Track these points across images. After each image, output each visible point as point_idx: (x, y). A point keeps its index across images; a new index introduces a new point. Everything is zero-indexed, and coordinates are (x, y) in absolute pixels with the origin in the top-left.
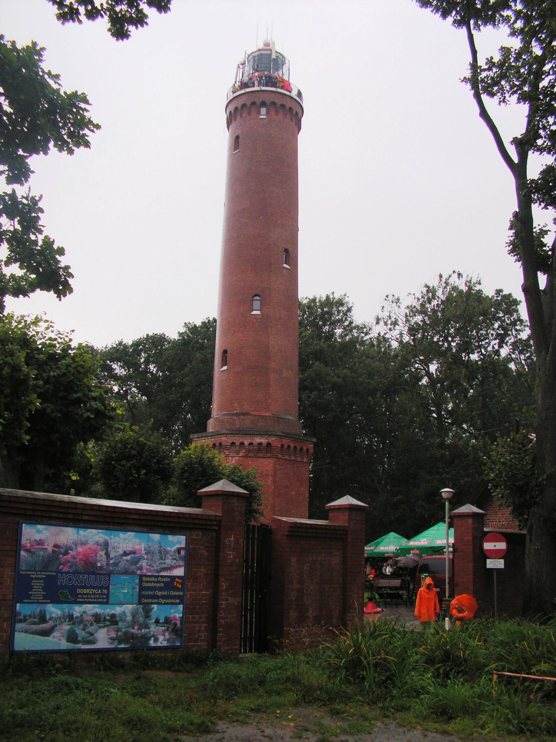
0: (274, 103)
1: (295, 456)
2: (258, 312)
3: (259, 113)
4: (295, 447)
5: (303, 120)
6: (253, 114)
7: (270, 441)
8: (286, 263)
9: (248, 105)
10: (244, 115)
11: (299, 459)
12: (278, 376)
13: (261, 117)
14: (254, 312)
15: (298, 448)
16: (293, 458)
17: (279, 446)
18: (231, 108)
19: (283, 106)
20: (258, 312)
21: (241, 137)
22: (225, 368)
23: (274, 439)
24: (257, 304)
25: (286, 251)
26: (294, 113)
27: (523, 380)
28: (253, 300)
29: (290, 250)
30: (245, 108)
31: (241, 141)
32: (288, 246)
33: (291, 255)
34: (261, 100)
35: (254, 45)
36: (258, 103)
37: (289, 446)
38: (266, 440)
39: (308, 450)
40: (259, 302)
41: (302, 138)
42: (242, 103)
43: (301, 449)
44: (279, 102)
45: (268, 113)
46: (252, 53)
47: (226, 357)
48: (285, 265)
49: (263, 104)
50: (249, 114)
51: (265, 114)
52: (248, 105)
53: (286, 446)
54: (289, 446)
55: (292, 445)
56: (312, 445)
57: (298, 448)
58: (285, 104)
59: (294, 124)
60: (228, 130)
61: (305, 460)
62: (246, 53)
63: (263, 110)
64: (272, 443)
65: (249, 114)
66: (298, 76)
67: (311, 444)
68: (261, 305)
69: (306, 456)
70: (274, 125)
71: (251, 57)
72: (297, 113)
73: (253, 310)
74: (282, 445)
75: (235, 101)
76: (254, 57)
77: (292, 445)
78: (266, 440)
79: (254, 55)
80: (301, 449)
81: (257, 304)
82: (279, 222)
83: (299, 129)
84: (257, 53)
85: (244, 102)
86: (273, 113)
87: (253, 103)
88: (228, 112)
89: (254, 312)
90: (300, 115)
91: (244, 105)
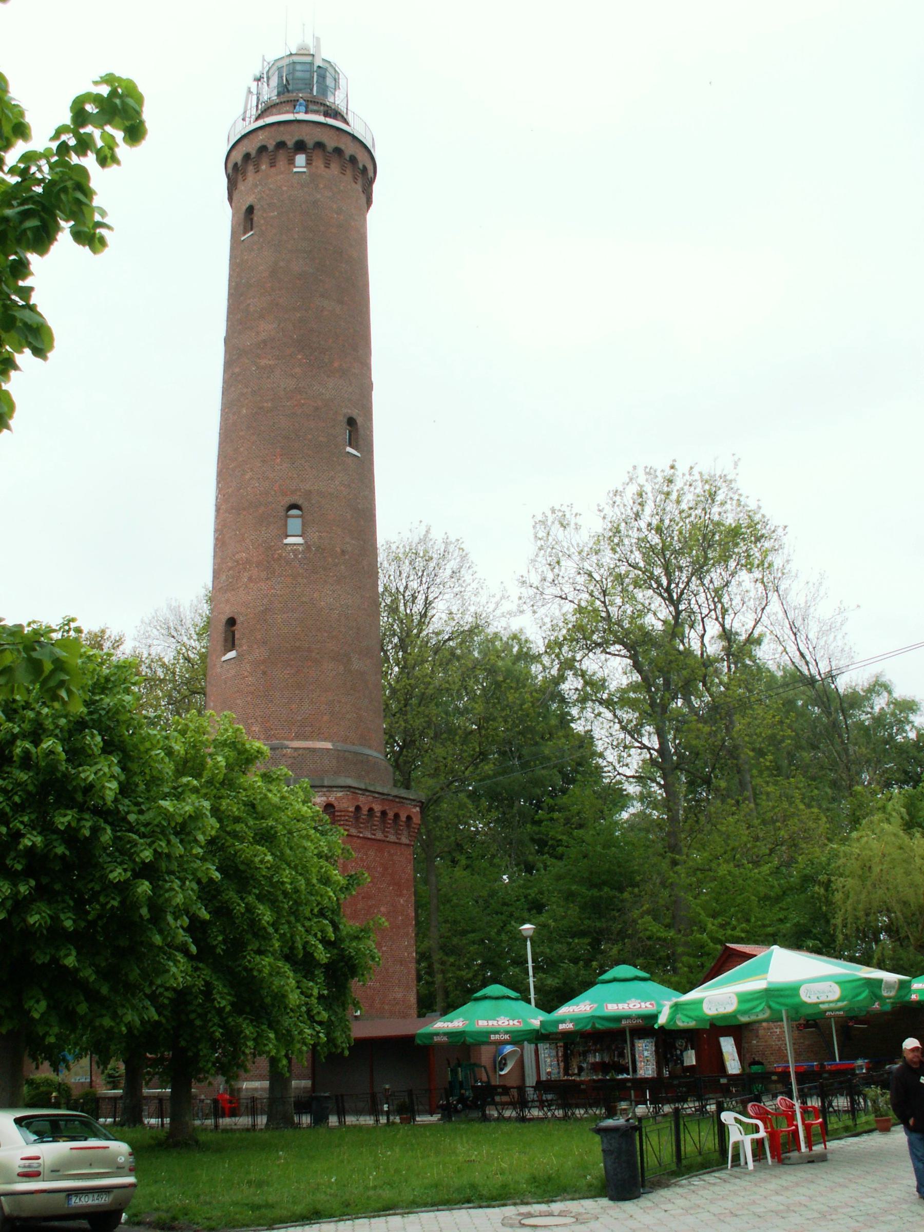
0: (320, 145)
1: (384, 831)
2: (300, 540)
3: (291, 162)
4: (384, 813)
5: (376, 187)
6: (282, 163)
7: (332, 799)
8: (350, 445)
9: (271, 147)
10: (263, 167)
11: (392, 838)
12: (341, 668)
13: (295, 170)
14: (290, 540)
15: (391, 815)
16: (379, 835)
17: (352, 809)
18: (237, 156)
19: (338, 151)
20: (300, 540)
21: (256, 207)
22: (232, 654)
23: (340, 794)
24: (295, 524)
25: (351, 422)
26: (361, 166)
27: (220, 758)
28: (287, 516)
29: (360, 421)
30: (264, 154)
31: (239, 630)
32: (355, 413)
33: (361, 431)
34: (296, 138)
35: (278, 47)
36: (290, 144)
37: (371, 810)
38: (324, 799)
39: (409, 818)
40: (299, 521)
41: (373, 217)
42: (259, 145)
43: (397, 816)
44: (331, 142)
45: (309, 162)
46: (276, 61)
47: (233, 632)
48: (349, 449)
49: (300, 147)
50: (273, 164)
51: (304, 164)
52: (271, 147)
53: (365, 811)
54: (371, 810)
55: (377, 808)
56: (418, 809)
57: (391, 815)
58: (343, 147)
59: (361, 190)
60: (230, 199)
61: (404, 840)
62: (264, 60)
63: (301, 159)
64: (336, 804)
65: (273, 164)
66: (365, 108)
67: (415, 806)
68: (303, 525)
69: (405, 833)
70: (322, 186)
71: (275, 68)
72: (364, 167)
73: (287, 536)
74: (358, 808)
75: (246, 141)
76: (280, 69)
77: (377, 808)
78: (324, 799)
79: (280, 64)
80: (397, 816)
81: (295, 524)
82: (336, 364)
83: (369, 202)
84: (287, 61)
85: (264, 143)
86: (319, 163)
87: (281, 145)
88: (230, 166)
89: (290, 540)
90: (371, 174)
91: (263, 149)
